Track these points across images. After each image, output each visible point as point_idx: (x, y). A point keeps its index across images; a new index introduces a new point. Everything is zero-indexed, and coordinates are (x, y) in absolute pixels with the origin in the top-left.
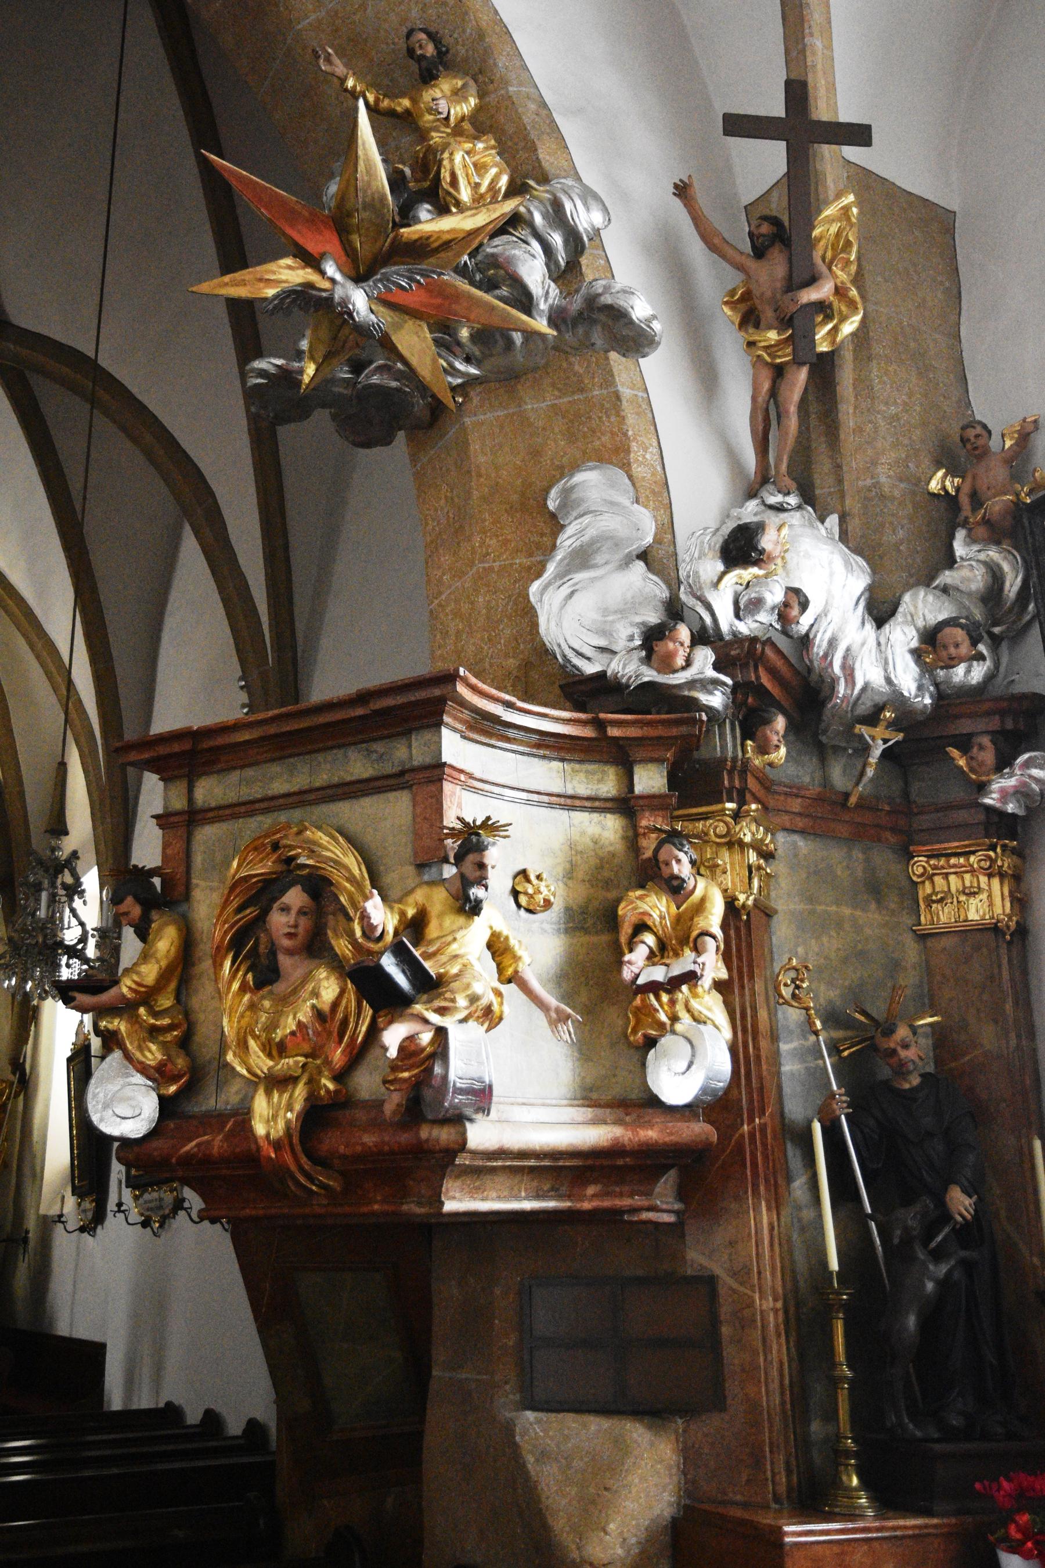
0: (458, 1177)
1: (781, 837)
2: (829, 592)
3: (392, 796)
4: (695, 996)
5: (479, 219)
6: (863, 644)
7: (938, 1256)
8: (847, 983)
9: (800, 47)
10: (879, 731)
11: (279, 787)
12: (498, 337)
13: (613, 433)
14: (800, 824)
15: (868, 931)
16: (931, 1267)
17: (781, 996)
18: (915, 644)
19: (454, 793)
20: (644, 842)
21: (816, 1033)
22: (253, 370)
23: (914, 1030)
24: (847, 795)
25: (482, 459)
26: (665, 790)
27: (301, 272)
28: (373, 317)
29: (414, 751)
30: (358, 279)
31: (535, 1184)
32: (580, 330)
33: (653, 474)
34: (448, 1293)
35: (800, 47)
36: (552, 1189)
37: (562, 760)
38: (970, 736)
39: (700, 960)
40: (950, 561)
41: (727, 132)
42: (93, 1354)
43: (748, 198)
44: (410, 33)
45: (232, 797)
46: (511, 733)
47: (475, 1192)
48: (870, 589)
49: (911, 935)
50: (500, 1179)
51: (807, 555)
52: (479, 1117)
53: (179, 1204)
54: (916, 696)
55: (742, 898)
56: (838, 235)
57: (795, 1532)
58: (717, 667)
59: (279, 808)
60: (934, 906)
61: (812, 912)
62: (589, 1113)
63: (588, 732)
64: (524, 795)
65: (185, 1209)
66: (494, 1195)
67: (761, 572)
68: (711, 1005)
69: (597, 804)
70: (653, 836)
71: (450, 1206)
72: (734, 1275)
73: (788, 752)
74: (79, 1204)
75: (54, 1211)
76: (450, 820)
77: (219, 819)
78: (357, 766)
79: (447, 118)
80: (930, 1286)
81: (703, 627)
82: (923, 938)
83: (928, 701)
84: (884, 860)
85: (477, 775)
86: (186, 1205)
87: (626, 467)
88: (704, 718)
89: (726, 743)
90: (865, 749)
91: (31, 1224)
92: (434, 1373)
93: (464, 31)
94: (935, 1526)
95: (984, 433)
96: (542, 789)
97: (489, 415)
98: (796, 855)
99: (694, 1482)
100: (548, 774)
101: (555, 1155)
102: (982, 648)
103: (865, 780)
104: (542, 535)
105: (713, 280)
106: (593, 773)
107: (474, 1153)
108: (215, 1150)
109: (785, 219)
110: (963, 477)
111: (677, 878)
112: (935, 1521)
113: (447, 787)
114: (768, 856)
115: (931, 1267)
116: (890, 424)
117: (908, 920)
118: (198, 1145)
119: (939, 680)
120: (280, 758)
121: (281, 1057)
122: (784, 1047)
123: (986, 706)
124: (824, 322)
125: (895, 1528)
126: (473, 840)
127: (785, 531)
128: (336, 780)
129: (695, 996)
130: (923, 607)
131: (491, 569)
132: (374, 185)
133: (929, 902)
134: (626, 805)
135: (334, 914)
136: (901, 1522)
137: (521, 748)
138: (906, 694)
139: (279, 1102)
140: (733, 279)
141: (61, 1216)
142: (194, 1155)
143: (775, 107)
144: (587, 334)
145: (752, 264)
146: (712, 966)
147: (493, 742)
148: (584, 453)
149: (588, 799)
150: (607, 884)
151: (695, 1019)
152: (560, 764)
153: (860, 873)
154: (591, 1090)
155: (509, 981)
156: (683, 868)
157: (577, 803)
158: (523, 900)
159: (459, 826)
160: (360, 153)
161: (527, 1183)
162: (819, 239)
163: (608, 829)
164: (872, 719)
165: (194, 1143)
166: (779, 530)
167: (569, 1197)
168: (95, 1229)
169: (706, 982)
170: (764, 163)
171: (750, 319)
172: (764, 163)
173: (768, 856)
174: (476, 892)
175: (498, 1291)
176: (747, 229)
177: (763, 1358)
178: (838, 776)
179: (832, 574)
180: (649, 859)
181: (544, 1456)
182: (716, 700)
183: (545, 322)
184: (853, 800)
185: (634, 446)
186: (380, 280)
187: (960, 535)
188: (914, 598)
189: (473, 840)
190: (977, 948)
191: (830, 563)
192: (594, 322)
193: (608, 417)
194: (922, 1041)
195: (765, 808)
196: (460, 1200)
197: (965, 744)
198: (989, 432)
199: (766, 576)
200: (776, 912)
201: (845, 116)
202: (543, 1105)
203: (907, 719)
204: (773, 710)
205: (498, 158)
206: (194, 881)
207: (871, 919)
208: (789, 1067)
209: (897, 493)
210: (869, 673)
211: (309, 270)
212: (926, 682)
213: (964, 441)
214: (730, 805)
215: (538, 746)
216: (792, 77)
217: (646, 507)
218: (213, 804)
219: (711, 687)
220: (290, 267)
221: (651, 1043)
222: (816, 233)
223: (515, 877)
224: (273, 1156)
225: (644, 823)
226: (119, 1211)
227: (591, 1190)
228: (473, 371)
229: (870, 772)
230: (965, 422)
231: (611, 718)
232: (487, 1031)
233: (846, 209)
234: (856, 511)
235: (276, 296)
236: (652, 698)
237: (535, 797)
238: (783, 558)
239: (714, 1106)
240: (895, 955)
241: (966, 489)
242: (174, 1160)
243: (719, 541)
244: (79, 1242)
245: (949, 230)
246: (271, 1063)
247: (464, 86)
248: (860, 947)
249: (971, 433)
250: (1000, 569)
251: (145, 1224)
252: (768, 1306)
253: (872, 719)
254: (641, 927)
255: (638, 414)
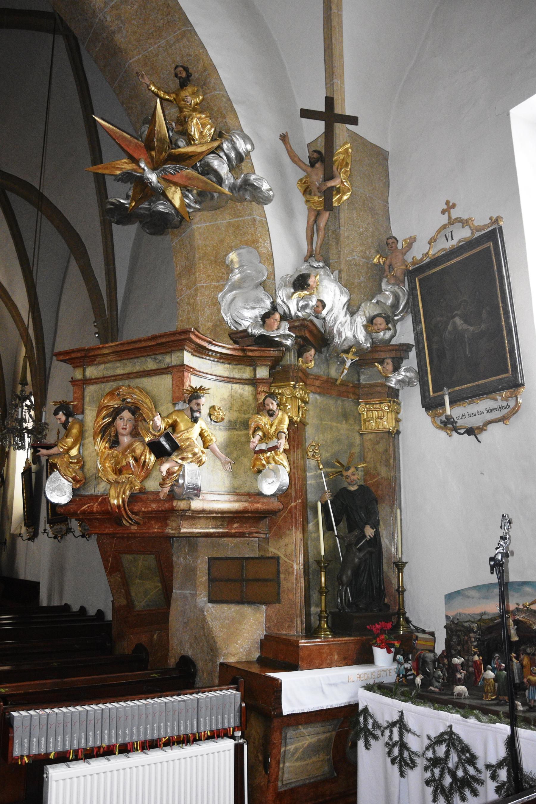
0: (186, 520)
1: (311, 395)
2: (334, 302)
3: (164, 376)
4: (277, 455)
5: (204, 148)
6: (346, 322)
7: (360, 550)
8: (333, 451)
9: (331, 83)
10: (350, 356)
11: (119, 371)
12: (208, 194)
13: (252, 234)
14: (318, 391)
15: (342, 432)
16: (358, 554)
17: (308, 455)
18: (365, 323)
19: (188, 376)
20: (259, 397)
21: (321, 469)
22: (109, 202)
23: (357, 469)
24: (336, 380)
25: (200, 242)
26: (268, 377)
27: (130, 165)
28: (159, 184)
29: (173, 359)
30: (154, 169)
31: (215, 523)
32: (241, 193)
33: (268, 252)
34: (180, 561)
35: (331, 83)
36: (221, 525)
37: (229, 364)
38: (384, 359)
39: (279, 442)
40: (380, 291)
41: (302, 116)
42: (35, 586)
43: (308, 141)
44: (176, 67)
45: (101, 375)
46: (210, 353)
47: (193, 526)
48: (349, 301)
49: (358, 433)
50: (202, 521)
51: (326, 287)
52: (195, 498)
53: (69, 530)
54: (365, 343)
55: (295, 418)
56: (343, 160)
57: (303, 643)
58: (289, 329)
59: (119, 380)
60: (367, 423)
61: (321, 424)
62: (236, 497)
63: (240, 354)
64: (214, 377)
65: (72, 532)
66: (200, 527)
67: (308, 293)
68: (283, 459)
69: (242, 381)
70: (263, 394)
71: (183, 530)
72: (286, 556)
73: (315, 363)
74: (27, 530)
75: (18, 532)
76: (187, 386)
77: (96, 383)
78: (151, 364)
79: (191, 104)
80: (357, 560)
81: (285, 313)
82: (361, 435)
83: (369, 345)
84: (349, 404)
85: (197, 369)
86: (72, 530)
87: (257, 248)
88: (284, 350)
89: (290, 359)
90: (343, 362)
91: (7, 537)
92: (174, 591)
93: (198, 67)
94: (352, 640)
95: (396, 241)
96: (221, 375)
97: (203, 225)
98: (316, 402)
99: (269, 627)
100: (222, 369)
101: (223, 512)
102: (390, 325)
103: (344, 374)
104: (223, 274)
105: (294, 174)
106: (241, 369)
107: (193, 511)
108: (95, 509)
109: (323, 152)
110: (386, 258)
111: (272, 410)
112: (352, 638)
113: (186, 374)
114: (305, 403)
115: (358, 554)
116: (360, 235)
117: (357, 428)
118: (88, 507)
119: (373, 337)
120: (120, 360)
121: (120, 475)
122: (308, 474)
123: (389, 348)
124: (337, 195)
125: (338, 641)
126: (195, 394)
127: (318, 277)
128: (142, 370)
129: (277, 455)
130: (369, 308)
131: (202, 286)
132: (162, 132)
133: (365, 421)
134: (253, 382)
135: (140, 421)
136: (341, 639)
137: (213, 359)
138: (361, 342)
139: (120, 491)
140: (302, 174)
141: (20, 534)
142: (87, 510)
143: (322, 108)
144: (244, 195)
145: (309, 169)
146: (283, 444)
147: (203, 356)
148: (241, 241)
149: (239, 379)
150: (245, 412)
151: (276, 463)
152: (228, 366)
153: (340, 410)
154: (236, 489)
155: (207, 448)
156: (274, 406)
157: (235, 381)
158: (213, 418)
159: (190, 389)
160: (157, 119)
161: (211, 523)
162: (336, 161)
163: (246, 391)
164: (347, 351)
165: (86, 506)
166: (315, 277)
167: (227, 528)
168: (34, 539)
169: (281, 450)
170: (315, 129)
171: (307, 191)
172: (315, 129)
173: (305, 403)
174: (197, 415)
175: (199, 562)
176: (308, 155)
177: (294, 582)
178: (333, 373)
179: (335, 295)
180: (261, 403)
181: (215, 619)
182: (289, 342)
183: (227, 189)
184: (338, 382)
185: (260, 240)
186: (163, 170)
187: (385, 280)
188: (366, 305)
189: (195, 394)
190: (382, 438)
191: (335, 290)
192: (246, 190)
193: (251, 228)
194: (360, 473)
195: (306, 384)
196: (187, 529)
197: (381, 362)
198: (397, 241)
199: (310, 295)
200: (308, 424)
201: (348, 112)
202: (219, 494)
203: (360, 351)
204: (310, 346)
205: (210, 121)
206: (85, 407)
207: (344, 427)
208: (310, 482)
209: (361, 263)
210: (347, 333)
211: (134, 164)
212: (368, 338)
213: (388, 244)
214: (292, 383)
215: (220, 358)
216: (328, 95)
217: (264, 264)
218: (93, 377)
219: (287, 337)
220: (126, 163)
221: (259, 471)
222: (335, 158)
223: (210, 409)
224: (117, 511)
225: (260, 389)
226: (45, 532)
227: (235, 525)
228: (198, 207)
229: (346, 372)
230: (388, 236)
231: (249, 349)
232: (199, 466)
233: (347, 150)
234: (345, 270)
235: (120, 174)
236: (264, 341)
237: (219, 378)
238: (317, 288)
239: (282, 495)
240: (352, 441)
241: (388, 263)
242: (79, 512)
243: (292, 280)
244: (27, 544)
245: (386, 159)
246: (116, 477)
247: (198, 91)
248: (338, 437)
249: (390, 241)
250: (399, 295)
251: (55, 537)
252: (299, 568)
253: (347, 351)
254: (258, 428)
255: (262, 227)
